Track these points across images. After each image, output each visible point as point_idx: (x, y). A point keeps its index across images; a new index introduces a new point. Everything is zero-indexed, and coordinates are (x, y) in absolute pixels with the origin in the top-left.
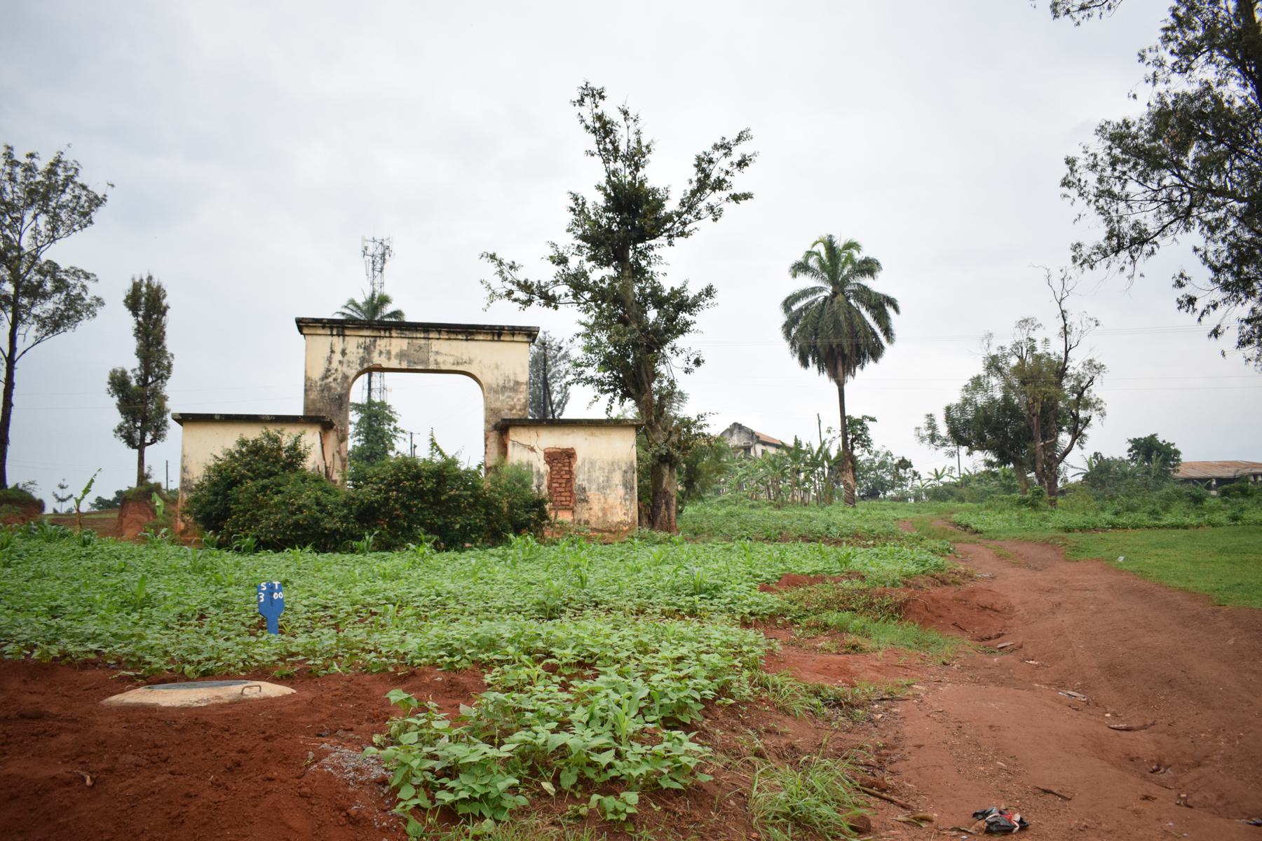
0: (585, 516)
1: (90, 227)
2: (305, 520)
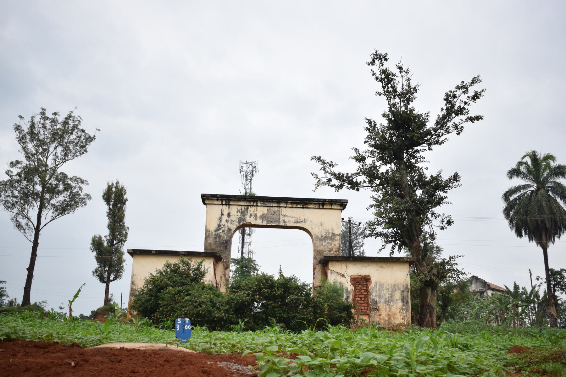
0: (377, 319)
1: (85, 154)
2: (203, 311)
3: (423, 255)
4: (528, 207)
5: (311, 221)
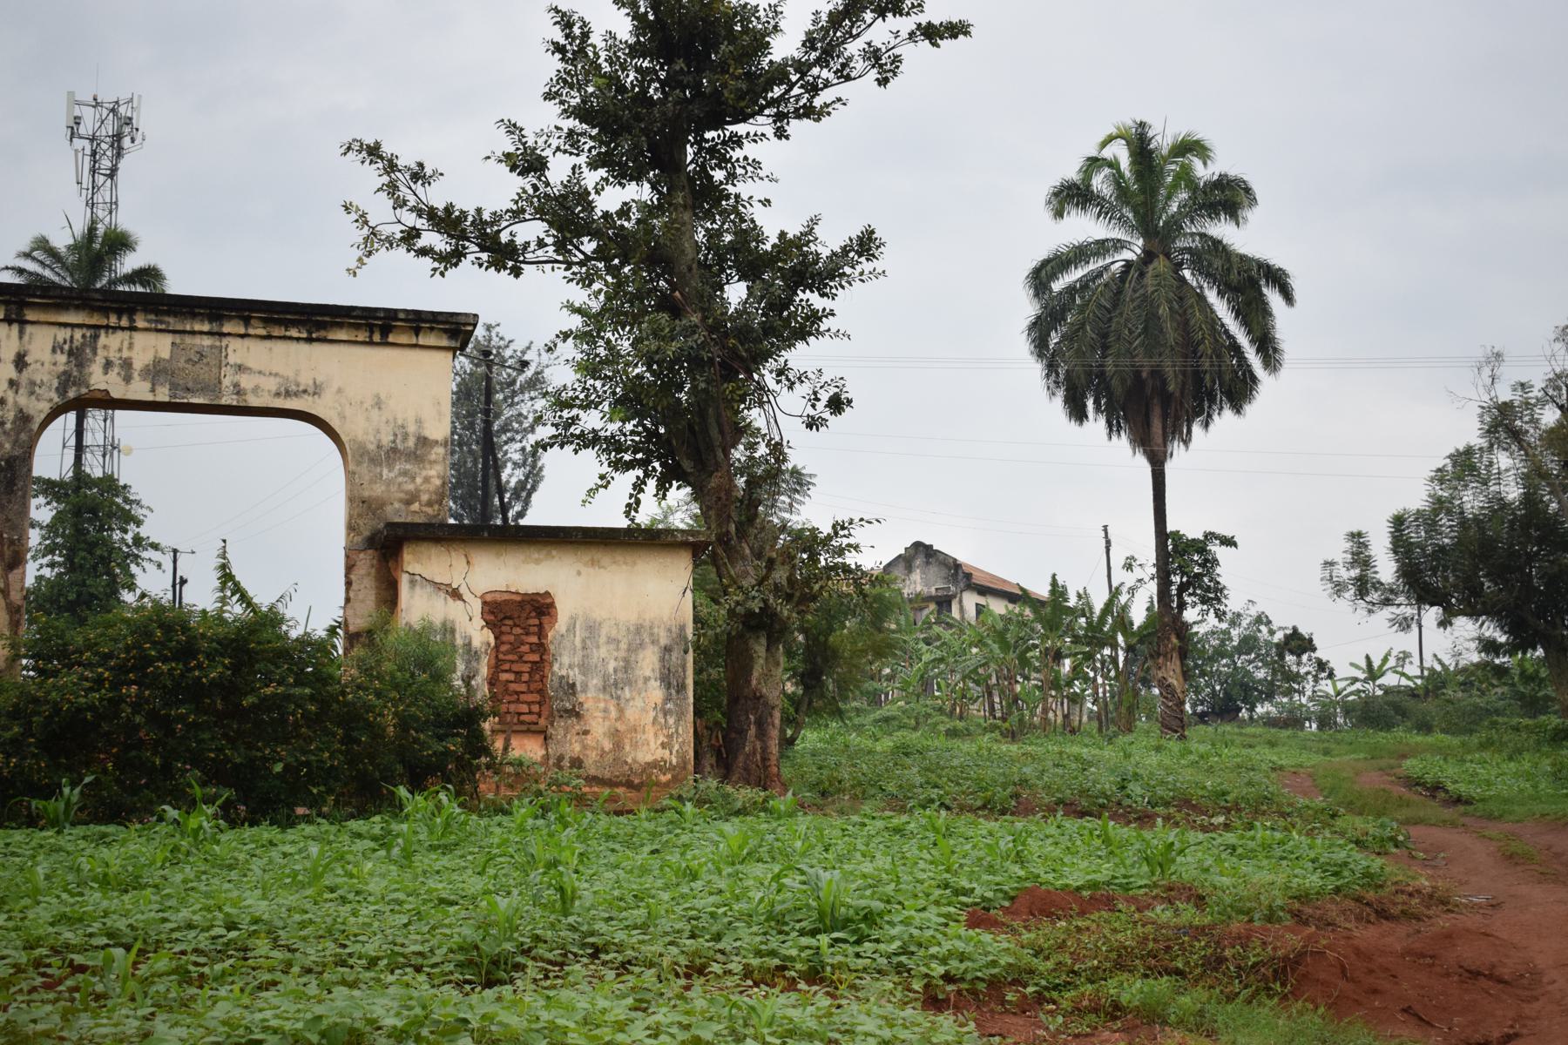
3: (743, 518)
4: (1110, 319)
5: (339, 391)
